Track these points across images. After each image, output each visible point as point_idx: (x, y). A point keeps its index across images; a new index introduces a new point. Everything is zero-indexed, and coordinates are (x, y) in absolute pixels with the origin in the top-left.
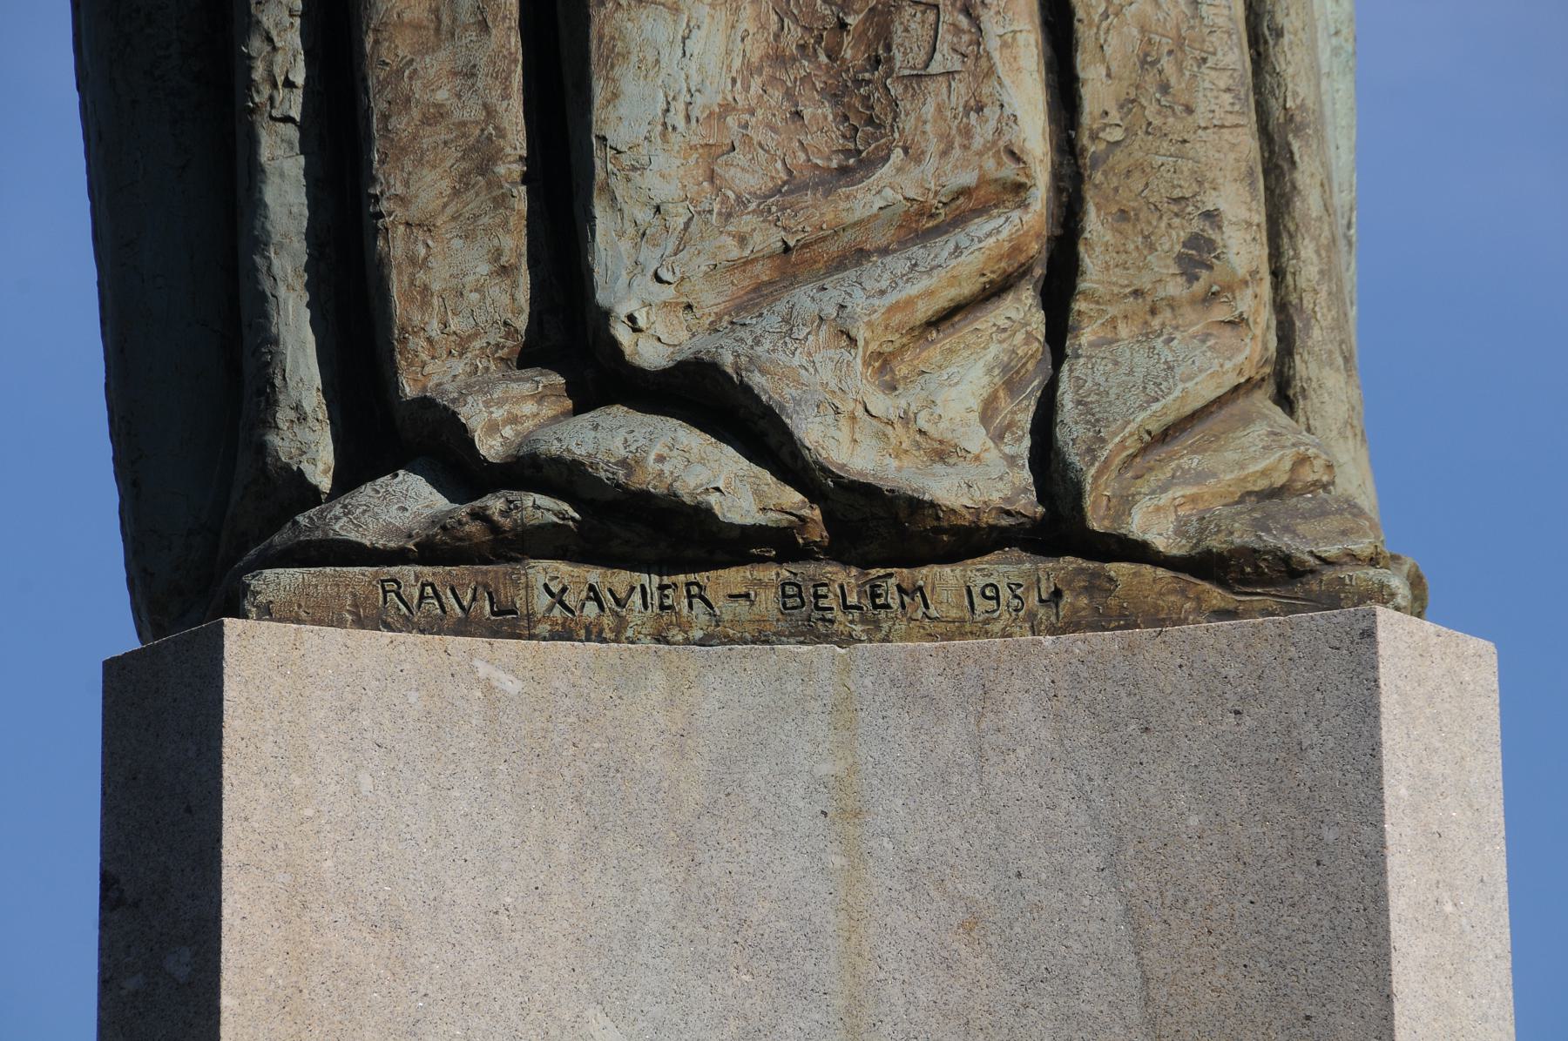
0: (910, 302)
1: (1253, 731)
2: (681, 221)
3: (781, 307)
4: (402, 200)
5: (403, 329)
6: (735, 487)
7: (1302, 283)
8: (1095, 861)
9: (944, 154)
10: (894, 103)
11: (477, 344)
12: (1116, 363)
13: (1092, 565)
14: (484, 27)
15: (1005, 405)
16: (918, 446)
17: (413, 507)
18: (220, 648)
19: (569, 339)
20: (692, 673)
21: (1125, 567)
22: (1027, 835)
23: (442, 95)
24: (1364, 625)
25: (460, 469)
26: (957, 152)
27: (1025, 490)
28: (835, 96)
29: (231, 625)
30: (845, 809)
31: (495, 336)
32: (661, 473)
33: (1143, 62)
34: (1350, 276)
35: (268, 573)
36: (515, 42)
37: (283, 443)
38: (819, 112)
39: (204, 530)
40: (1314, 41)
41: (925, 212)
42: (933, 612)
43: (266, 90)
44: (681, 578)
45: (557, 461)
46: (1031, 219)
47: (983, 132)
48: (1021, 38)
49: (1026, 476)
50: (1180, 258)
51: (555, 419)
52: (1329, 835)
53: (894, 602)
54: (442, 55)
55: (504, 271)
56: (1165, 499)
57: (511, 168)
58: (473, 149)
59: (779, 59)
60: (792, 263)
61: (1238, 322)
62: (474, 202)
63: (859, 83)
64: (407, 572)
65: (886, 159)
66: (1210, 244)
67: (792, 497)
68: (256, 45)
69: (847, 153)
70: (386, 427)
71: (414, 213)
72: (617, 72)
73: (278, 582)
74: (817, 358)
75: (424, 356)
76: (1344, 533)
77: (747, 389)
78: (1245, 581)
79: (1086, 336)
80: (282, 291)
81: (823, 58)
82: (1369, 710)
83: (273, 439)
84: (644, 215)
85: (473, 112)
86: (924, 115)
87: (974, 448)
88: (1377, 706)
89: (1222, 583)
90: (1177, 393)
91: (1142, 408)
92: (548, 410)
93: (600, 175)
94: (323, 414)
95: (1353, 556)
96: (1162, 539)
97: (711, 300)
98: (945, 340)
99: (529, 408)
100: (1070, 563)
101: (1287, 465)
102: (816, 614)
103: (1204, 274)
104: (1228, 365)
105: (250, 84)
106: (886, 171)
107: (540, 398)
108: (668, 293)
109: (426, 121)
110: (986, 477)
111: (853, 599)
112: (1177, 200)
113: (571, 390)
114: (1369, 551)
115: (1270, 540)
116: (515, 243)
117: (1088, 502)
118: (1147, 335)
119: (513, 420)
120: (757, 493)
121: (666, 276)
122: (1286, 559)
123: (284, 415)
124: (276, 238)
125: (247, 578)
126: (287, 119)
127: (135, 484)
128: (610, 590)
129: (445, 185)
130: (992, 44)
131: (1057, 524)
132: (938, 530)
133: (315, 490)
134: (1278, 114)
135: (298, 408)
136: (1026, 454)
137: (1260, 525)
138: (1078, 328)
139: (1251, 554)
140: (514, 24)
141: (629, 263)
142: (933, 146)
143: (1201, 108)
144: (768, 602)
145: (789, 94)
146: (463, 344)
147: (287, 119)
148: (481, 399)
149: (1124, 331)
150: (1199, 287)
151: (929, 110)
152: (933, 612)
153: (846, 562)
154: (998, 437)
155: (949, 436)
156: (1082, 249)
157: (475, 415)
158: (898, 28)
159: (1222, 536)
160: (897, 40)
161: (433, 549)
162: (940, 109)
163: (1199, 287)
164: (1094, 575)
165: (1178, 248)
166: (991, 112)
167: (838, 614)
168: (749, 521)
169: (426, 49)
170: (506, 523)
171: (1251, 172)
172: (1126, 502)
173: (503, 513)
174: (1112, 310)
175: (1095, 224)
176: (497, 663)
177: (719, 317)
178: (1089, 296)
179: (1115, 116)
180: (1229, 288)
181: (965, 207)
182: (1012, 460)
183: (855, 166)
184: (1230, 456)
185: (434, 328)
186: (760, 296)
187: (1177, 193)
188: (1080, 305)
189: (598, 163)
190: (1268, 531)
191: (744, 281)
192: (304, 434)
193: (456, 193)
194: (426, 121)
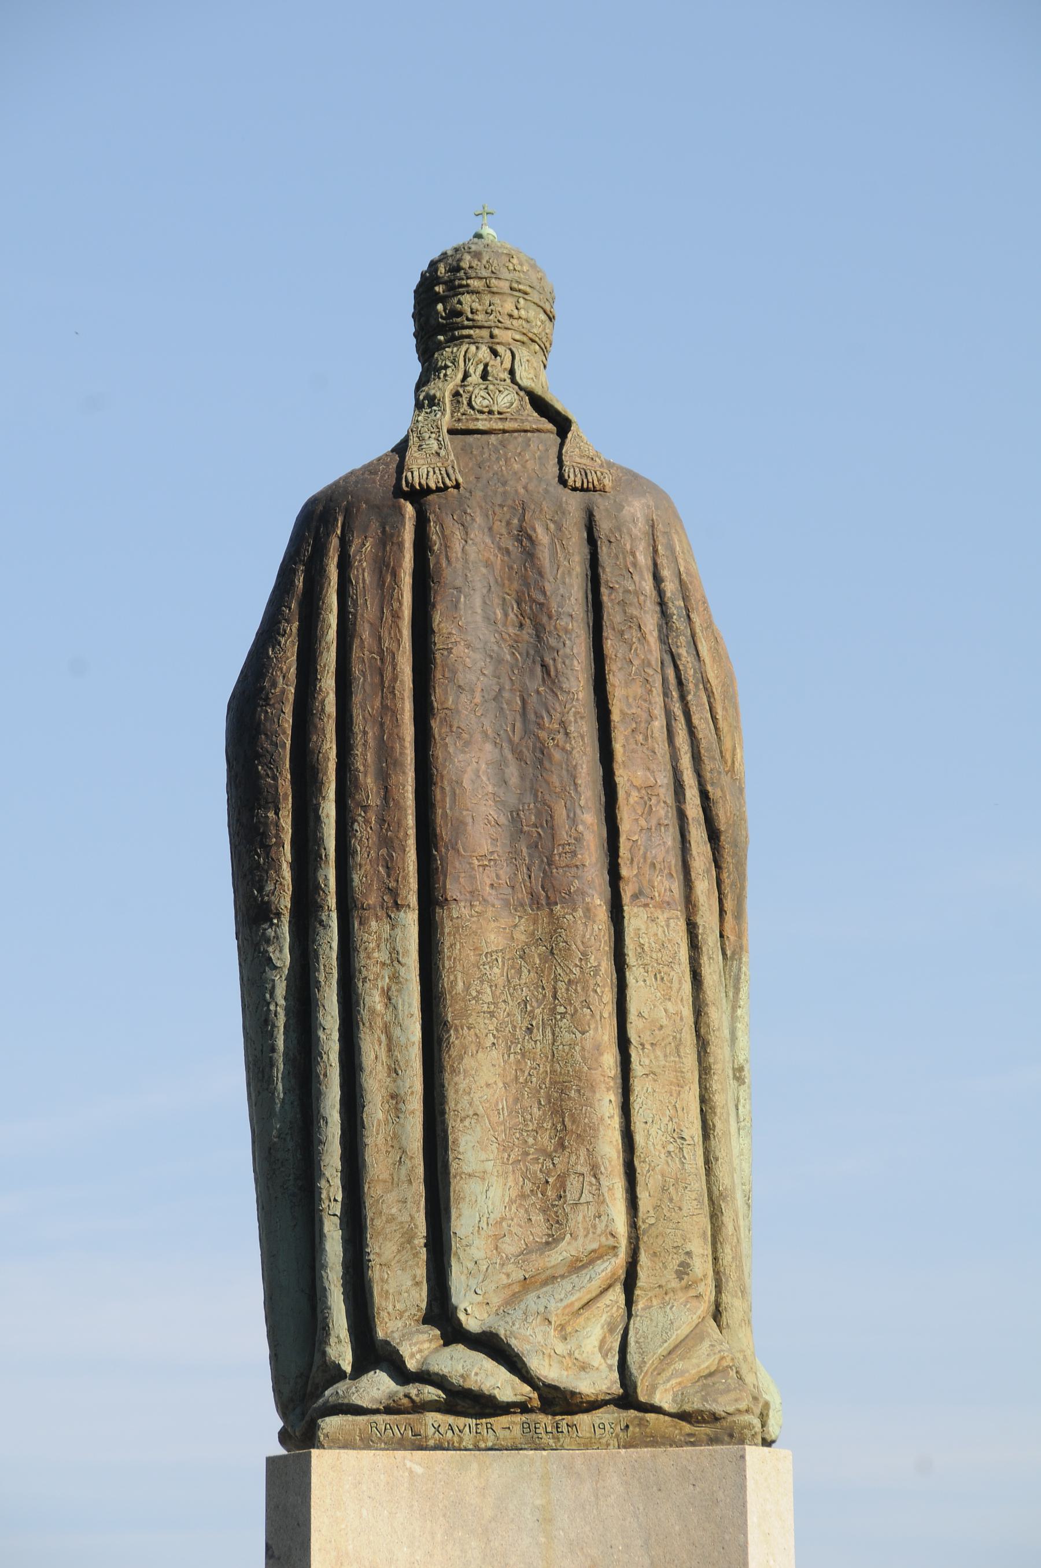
0: (572, 1304)
1: (700, 1493)
2: (485, 1267)
3: (523, 1306)
4: (378, 1254)
5: (378, 1309)
7: (725, 1263)
8: (640, 1542)
9: (586, 1236)
10: (567, 1215)
11: (407, 1314)
12: (651, 1320)
13: (641, 1414)
14: (410, 1182)
15: (609, 1339)
16: (575, 1364)
17: (382, 1388)
18: (310, 1462)
19: (441, 1314)
20: (488, 1463)
21: (653, 1415)
22: (614, 1531)
23: (394, 1211)
24: (741, 1453)
26: (591, 1235)
27: (616, 1382)
28: (544, 1211)
29: (315, 1452)
30: (546, 1519)
31: (414, 1311)
32: (476, 1381)
33: (663, 1190)
35: (327, 1419)
36: (422, 1188)
38: (538, 1218)
39: (305, 1399)
40: (731, 1159)
41: (578, 1260)
42: (580, 1435)
43: (327, 1202)
44: (484, 1421)
45: (437, 1374)
46: (618, 1262)
47: (601, 1227)
48: (616, 1186)
49: (616, 1375)
50: (677, 1272)
51: (436, 1350)
52: (727, 1537)
53: (565, 1430)
54: (394, 1193)
55: (417, 1284)
56: (669, 1385)
57: (420, 1241)
58: (406, 1233)
59: (523, 1196)
61: (698, 1297)
62: (406, 1255)
63: (553, 1206)
64: (379, 1418)
65: (564, 1239)
66: (688, 1265)
67: (527, 1389)
68: (323, 1184)
69: (549, 1235)
70: (373, 1354)
71: (383, 1260)
72: (461, 1205)
73: (331, 1424)
74: (536, 1331)
75: (387, 1320)
76: (736, 1400)
77: (509, 1346)
78: (698, 1422)
79: (639, 1306)
80: (332, 1287)
81: (540, 1195)
82: (742, 1488)
83: (328, 1350)
84: (471, 1265)
85: (405, 1218)
86: (578, 1220)
87: (596, 1364)
88: (745, 1486)
89: (690, 1423)
90: (674, 1337)
91: (661, 1346)
92: (434, 1345)
93: (454, 1248)
94: (348, 1339)
95: (739, 1411)
96: (666, 1406)
97: (496, 1301)
98: (586, 1314)
99: (426, 1345)
100: (633, 1413)
101: (716, 1362)
102: (535, 1436)
103: (686, 1277)
104: (695, 1317)
105: (321, 1199)
106: (564, 1244)
107: (430, 1341)
108: (480, 1298)
109: (388, 1221)
110: (599, 1380)
111: (549, 1429)
112: (675, 1248)
113: (443, 1336)
114: (746, 1407)
115: (708, 1407)
116: (421, 1272)
117: (639, 1390)
118: (664, 1304)
119: (420, 1351)
120: (513, 1388)
121: (479, 1292)
122: (714, 1414)
123: (333, 1340)
124: (330, 1265)
125: (319, 1421)
126: (335, 1215)
127: (276, 1355)
129: (395, 1248)
130: (604, 1190)
131: (627, 1398)
132: (582, 1402)
133: (345, 1372)
134: (716, 1193)
135: (338, 1337)
136: (616, 1364)
137: (704, 1399)
138: (637, 1301)
139: (701, 1412)
140: (422, 1181)
141: (465, 1286)
142: (581, 1233)
143: (685, 1209)
144: (517, 1430)
145: (526, 1211)
146: (401, 1314)
147: (335, 1215)
148: (408, 1343)
149: (655, 1302)
150: (684, 1283)
151: (580, 1218)
152: (580, 1435)
153: (547, 1414)
154: (605, 1356)
155: (586, 1360)
156: (639, 1269)
158: (568, 1184)
159: (690, 1405)
160: (568, 1189)
162: (584, 1217)
163: (684, 1283)
164: (641, 1419)
165: (676, 1267)
166: (604, 1218)
167: (544, 1435)
168: (510, 1400)
169: (387, 1191)
170: (417, 1399)
171: (704, 1233)
172: (653, 1388)
173: (417, 1395)
174: (650, 1294)
175: (644, 1258)
176: (414, 1461)
177: (499, 1307)
178: (641, 1289)
179: (652, 1213)
180: (695, 1282)
181: (594, 1257)
182: (610, 1367)
183: (553, 1241)
184: (694, 1361)
185: (390, 1308)
186: (513, 1299)
187: (675, 1245)
188: (637, 1292)
189: (453, 1243)
190: (707, 1402)
191: (509, 1292)
192: (341, 1348)
193: (399, 1251)
194: (388, 1221)
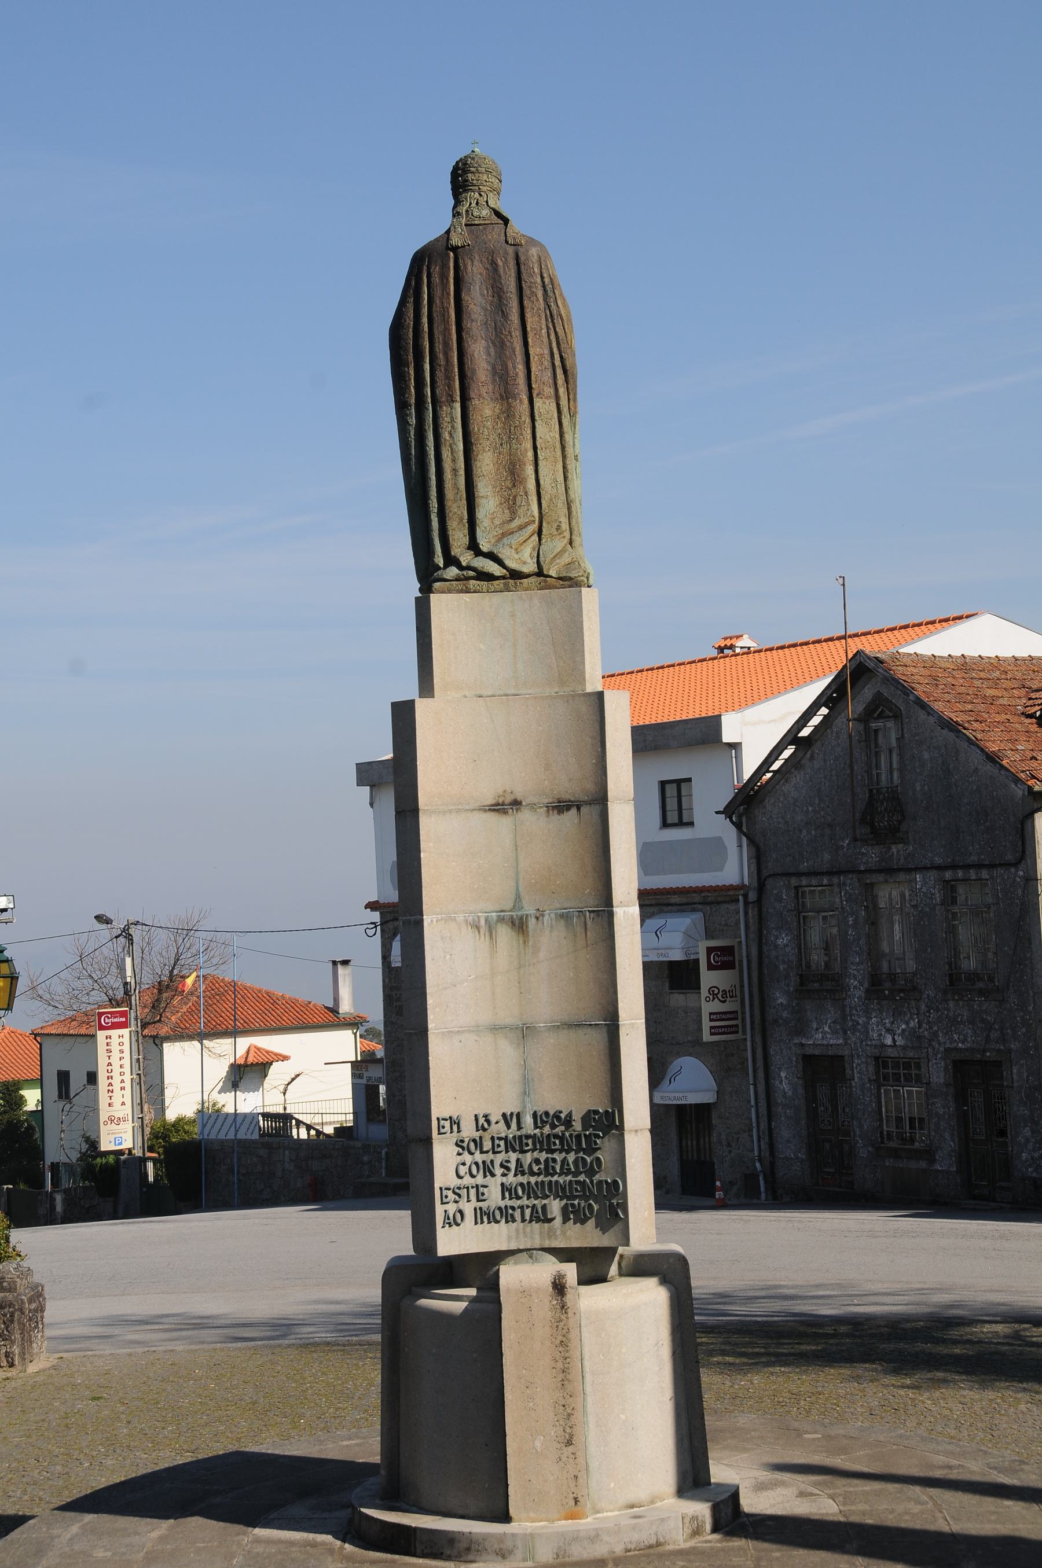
6: (495, 569)
19: (474, 546)
25: (460, 567)
29: (431, 595)
30: (513, 615)
34: (736, 1560)
37: (436, 560)
39: (428, 577)
60: (504, 535)
70: (451, 560)
73: (437, 585)
82: (581, 602)
86: (521, 511)
97: (493, 541)
110: (530, 567)
116: (466, 532)
128: (812, 1494)
131: (540, 573)
144: (502, 585)
157: (462, 559)
161: (457, 579)
175: (544, 524)
183: (512, 520)
186: (499, 540)
